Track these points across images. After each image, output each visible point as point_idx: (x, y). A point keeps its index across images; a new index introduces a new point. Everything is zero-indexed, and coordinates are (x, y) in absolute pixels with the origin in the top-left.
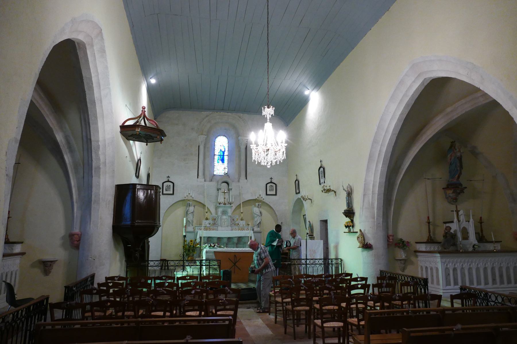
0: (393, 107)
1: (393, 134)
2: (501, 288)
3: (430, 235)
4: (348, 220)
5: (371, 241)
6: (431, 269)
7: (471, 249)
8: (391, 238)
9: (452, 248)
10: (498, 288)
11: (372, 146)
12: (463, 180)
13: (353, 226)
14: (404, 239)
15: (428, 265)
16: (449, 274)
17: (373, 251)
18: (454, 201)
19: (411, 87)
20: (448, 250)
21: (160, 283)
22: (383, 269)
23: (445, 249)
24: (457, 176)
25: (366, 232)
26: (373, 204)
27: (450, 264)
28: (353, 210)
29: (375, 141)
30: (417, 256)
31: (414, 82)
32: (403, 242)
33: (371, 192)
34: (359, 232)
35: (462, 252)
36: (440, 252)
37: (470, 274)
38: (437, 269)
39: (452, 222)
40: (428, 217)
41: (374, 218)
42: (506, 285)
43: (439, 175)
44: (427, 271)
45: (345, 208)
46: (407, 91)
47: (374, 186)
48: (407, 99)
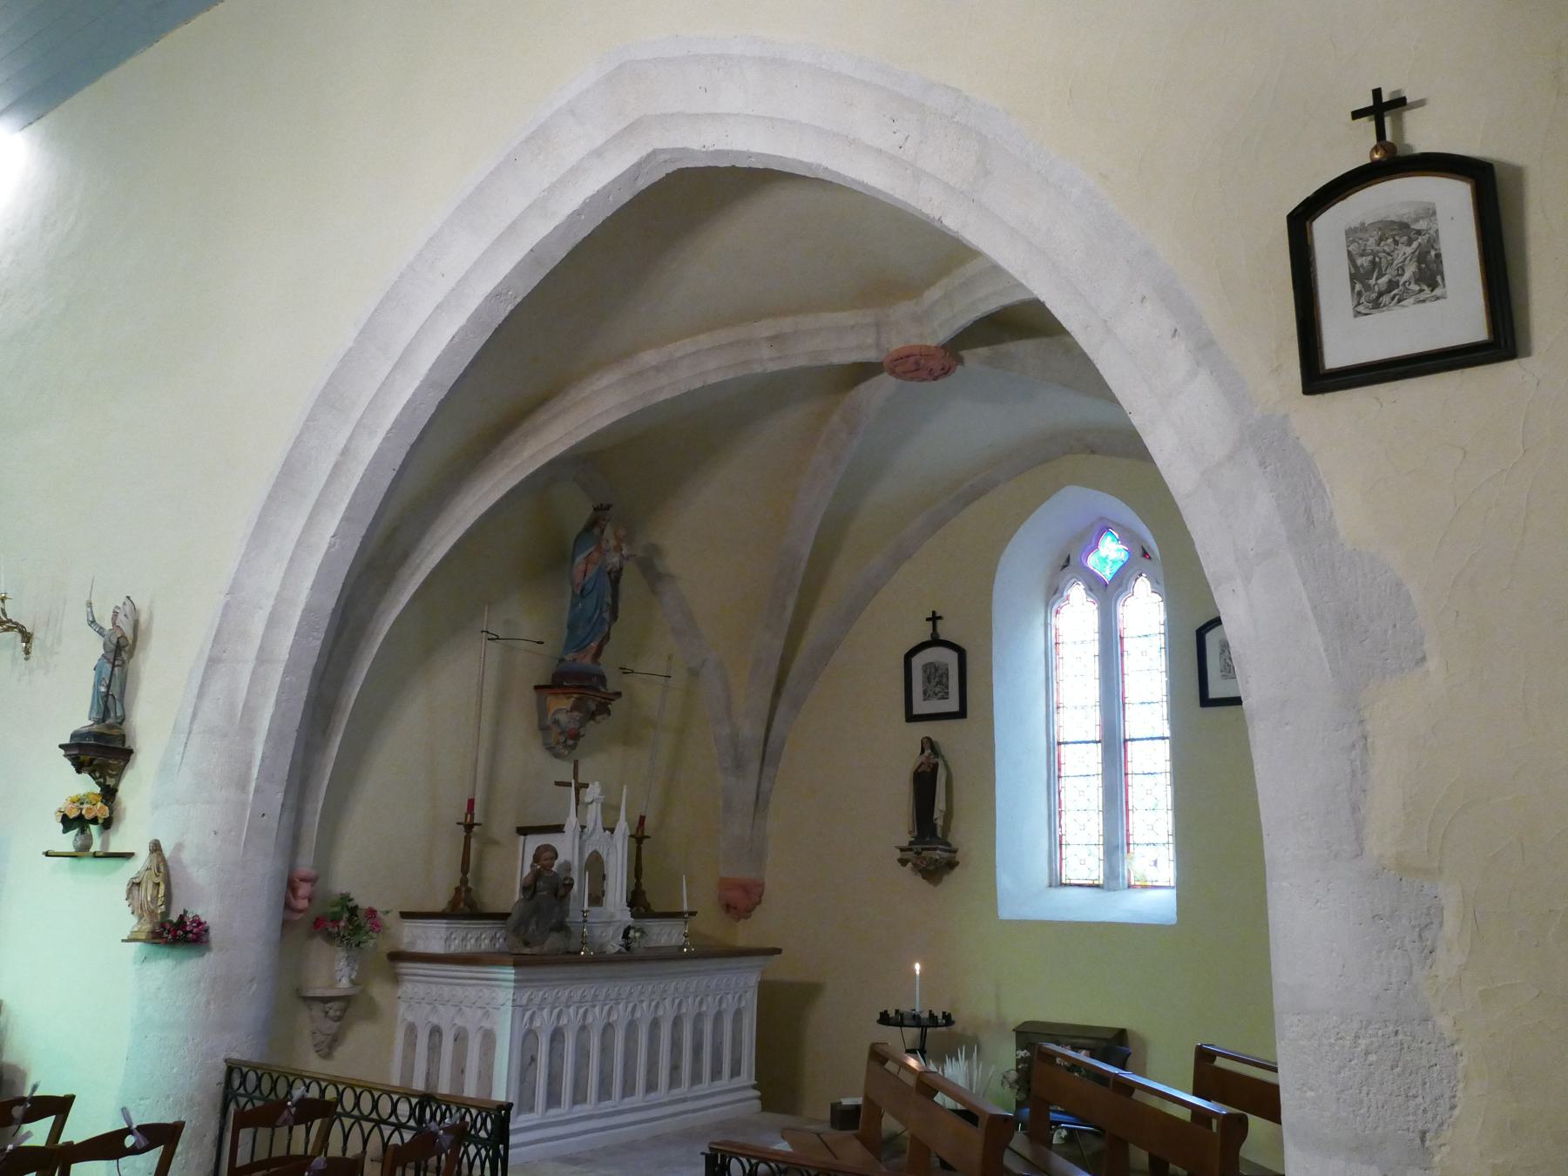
0: (465, 250)
1: (428, 383)
2: (737, 1090)
3: (464, 881)
4: (86, 785)
5: (203, 899)
6: (460, 1038)
8: (304, 889)
9: (554, 941)
10: (685, 1100)
11: (311, 418)
13: (107, 824)
14: (363, 901)
15: (445, 1018)
16: (533, 1059)
17: (210, 957)
19: (577, 175)
20: (536, 950)
22: (244, 1051)
23: (527, 944)
24: (594, 645)
25: (186, 856)
26: (249, 710)
27: (597, 1009)
28: (123, 738)
29: (330, 399)
30: (396, 979)
31: (598, 153)
32: (353, 911)
33: (251, 652)
34: (143, 858)
35: (588, 961)
36: (519, 962)
37: (606, 1050)
38: (489, 1038)
39: (558, 829)
40: (471, 803)
41: (242, 785)
42: (705, 1087)
43: (530, 626)
44: (434, 1049)
45: (80, 717)
46: (551, 189)
47: (273, 622)
48: (539, 230)
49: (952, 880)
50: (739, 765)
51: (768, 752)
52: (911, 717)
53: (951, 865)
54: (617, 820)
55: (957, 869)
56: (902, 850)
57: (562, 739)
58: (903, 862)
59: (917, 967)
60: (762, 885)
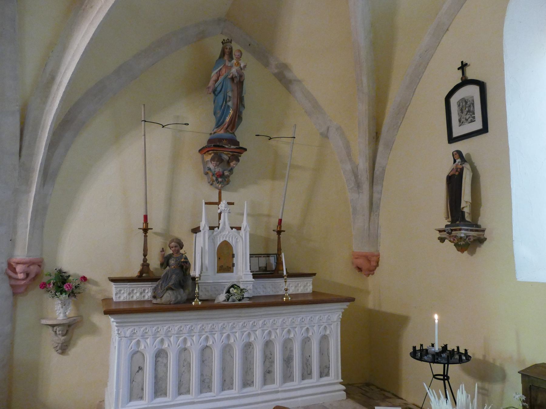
2: (320, 386)
3: (145, 260)
7: (222, 298)
10: (278, 392)
12: (243, 135)
18: (221, 180)
21: (434, 320)
37: (204, 361)
42: (296, 383)
49: (483, 250)
50: (358, 185)
51: (374, 176)
52: (452, 139)
53: (481, 241)
54: (242, 222)
55: (486, 243)
56: (440, 231)
57: (214, 178)
58: (442, 240)
59: (436, 317)
60: (378, 256)
